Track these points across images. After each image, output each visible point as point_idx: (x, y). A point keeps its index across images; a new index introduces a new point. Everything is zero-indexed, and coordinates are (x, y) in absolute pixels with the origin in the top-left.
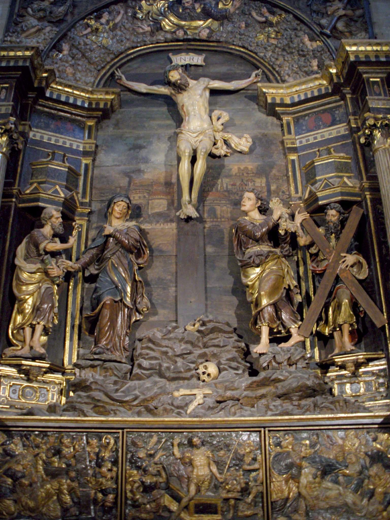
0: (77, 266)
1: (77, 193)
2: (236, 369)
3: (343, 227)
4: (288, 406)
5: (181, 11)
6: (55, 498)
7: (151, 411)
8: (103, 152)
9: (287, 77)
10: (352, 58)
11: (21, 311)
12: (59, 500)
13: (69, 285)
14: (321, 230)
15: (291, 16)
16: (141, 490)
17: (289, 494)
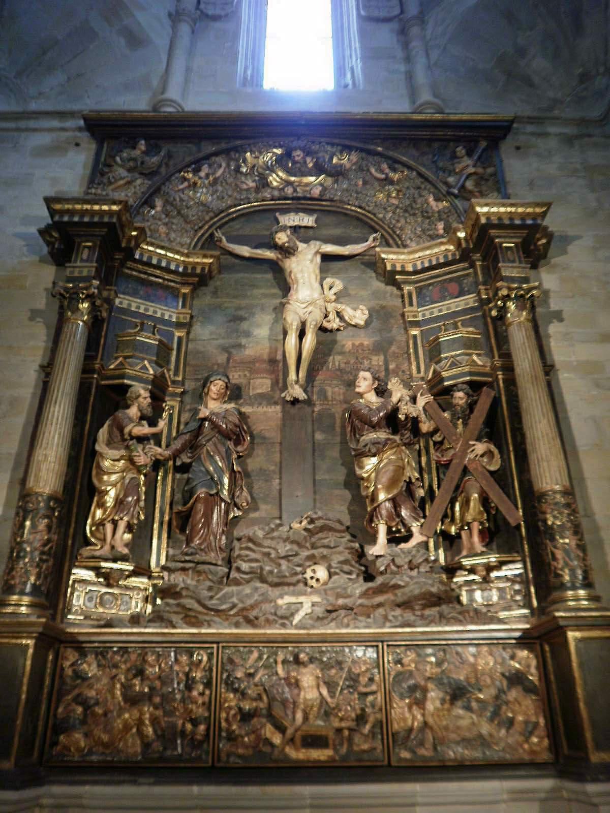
0: (167, 453)
1: (169, 370)
2: (350, 573)
3: (472, 411)
4: (409, 616)
6: (134, 730)
7: (251, 622)
9: (408, 242)
10: (483, 220)
11: (102, 505)
12: (140, 732)
13: (157, 475)
14: (446, 415)
15: (414, 173)
16: (239, 718)
17: (413, 723)
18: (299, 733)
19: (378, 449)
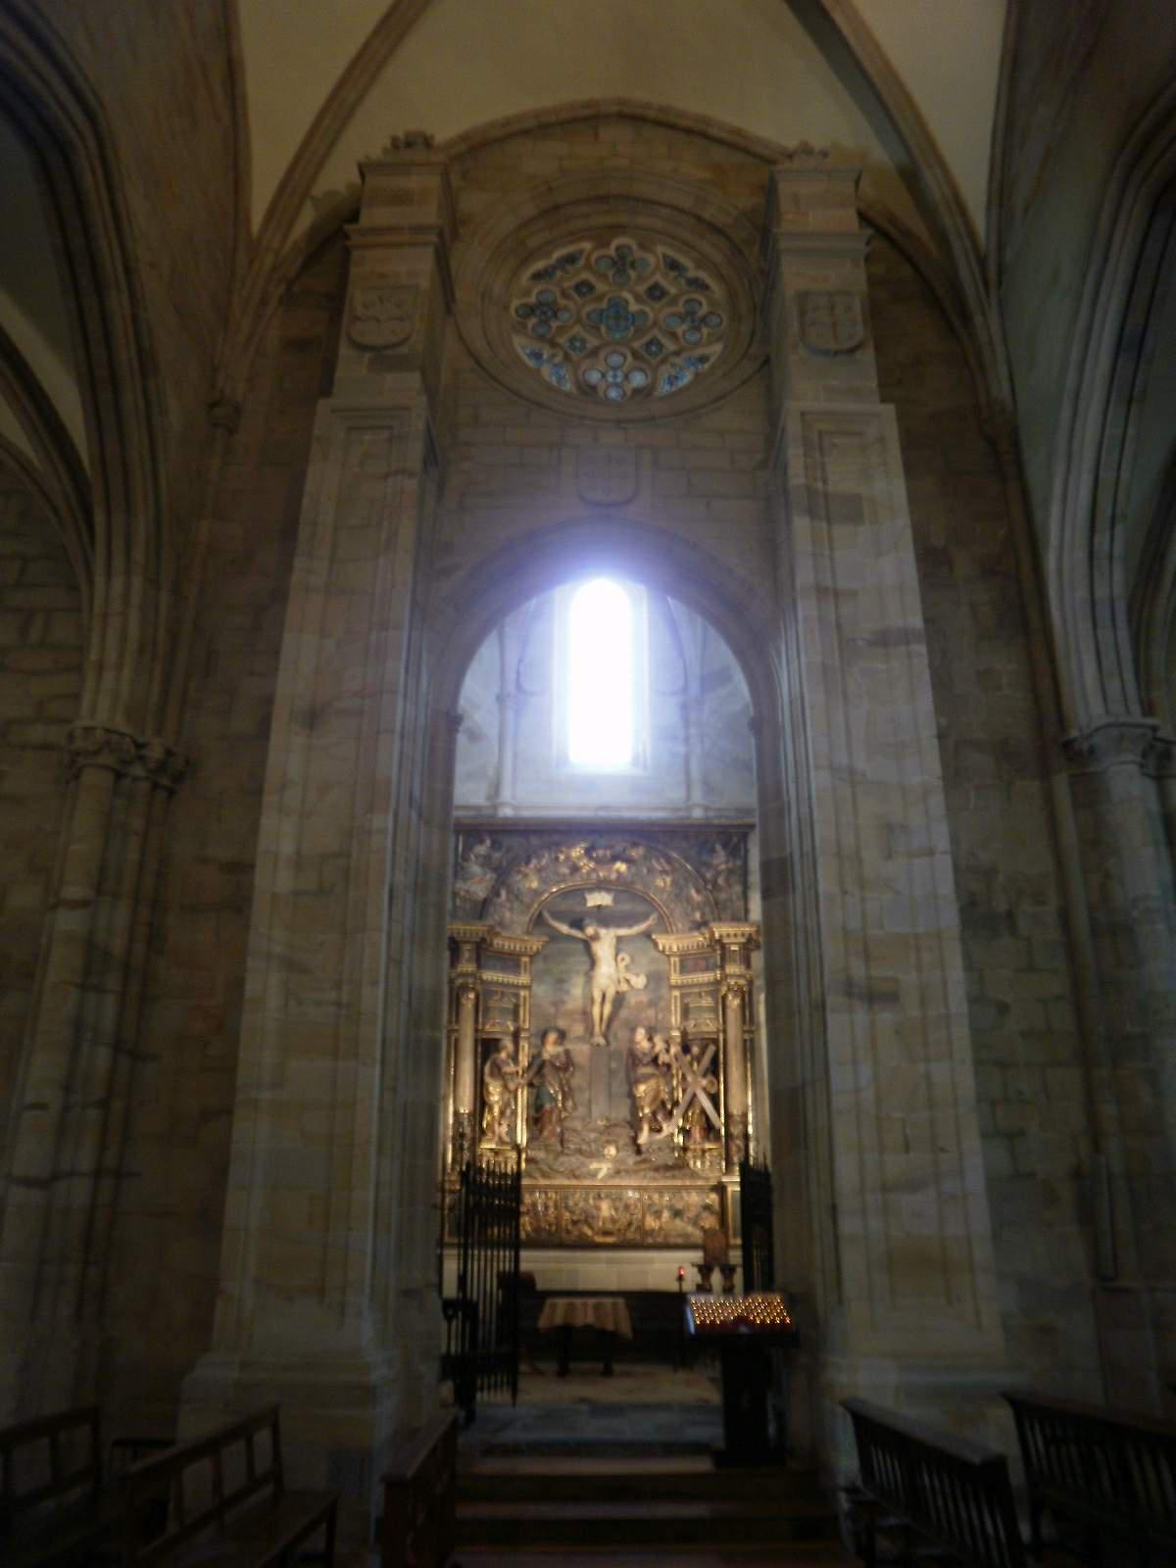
4: (657, 1175)
7: (576, 1177)
19: (645, 1078)
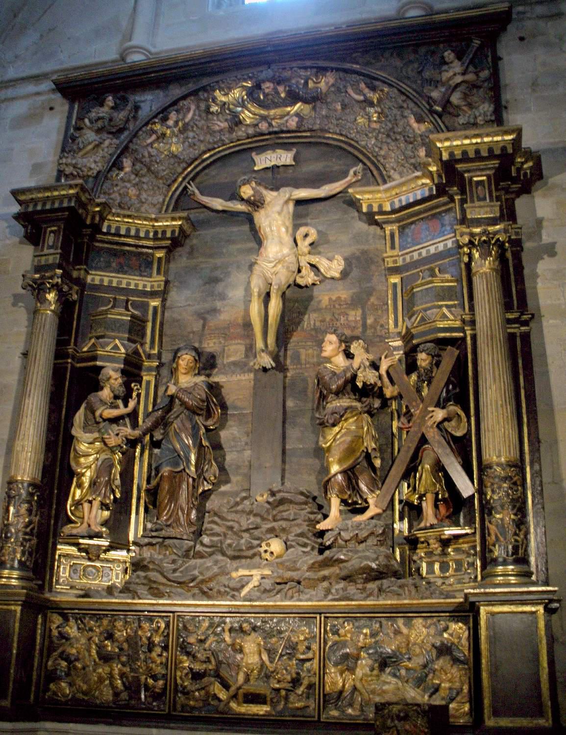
1: (142, 345)
2: (305, 545)
4: (352, 589)
5: (262, 97)
6: (107, 682)
8: (175, 289)
11: (80, 486)
13: (135, 452)
18: (241, 691)
